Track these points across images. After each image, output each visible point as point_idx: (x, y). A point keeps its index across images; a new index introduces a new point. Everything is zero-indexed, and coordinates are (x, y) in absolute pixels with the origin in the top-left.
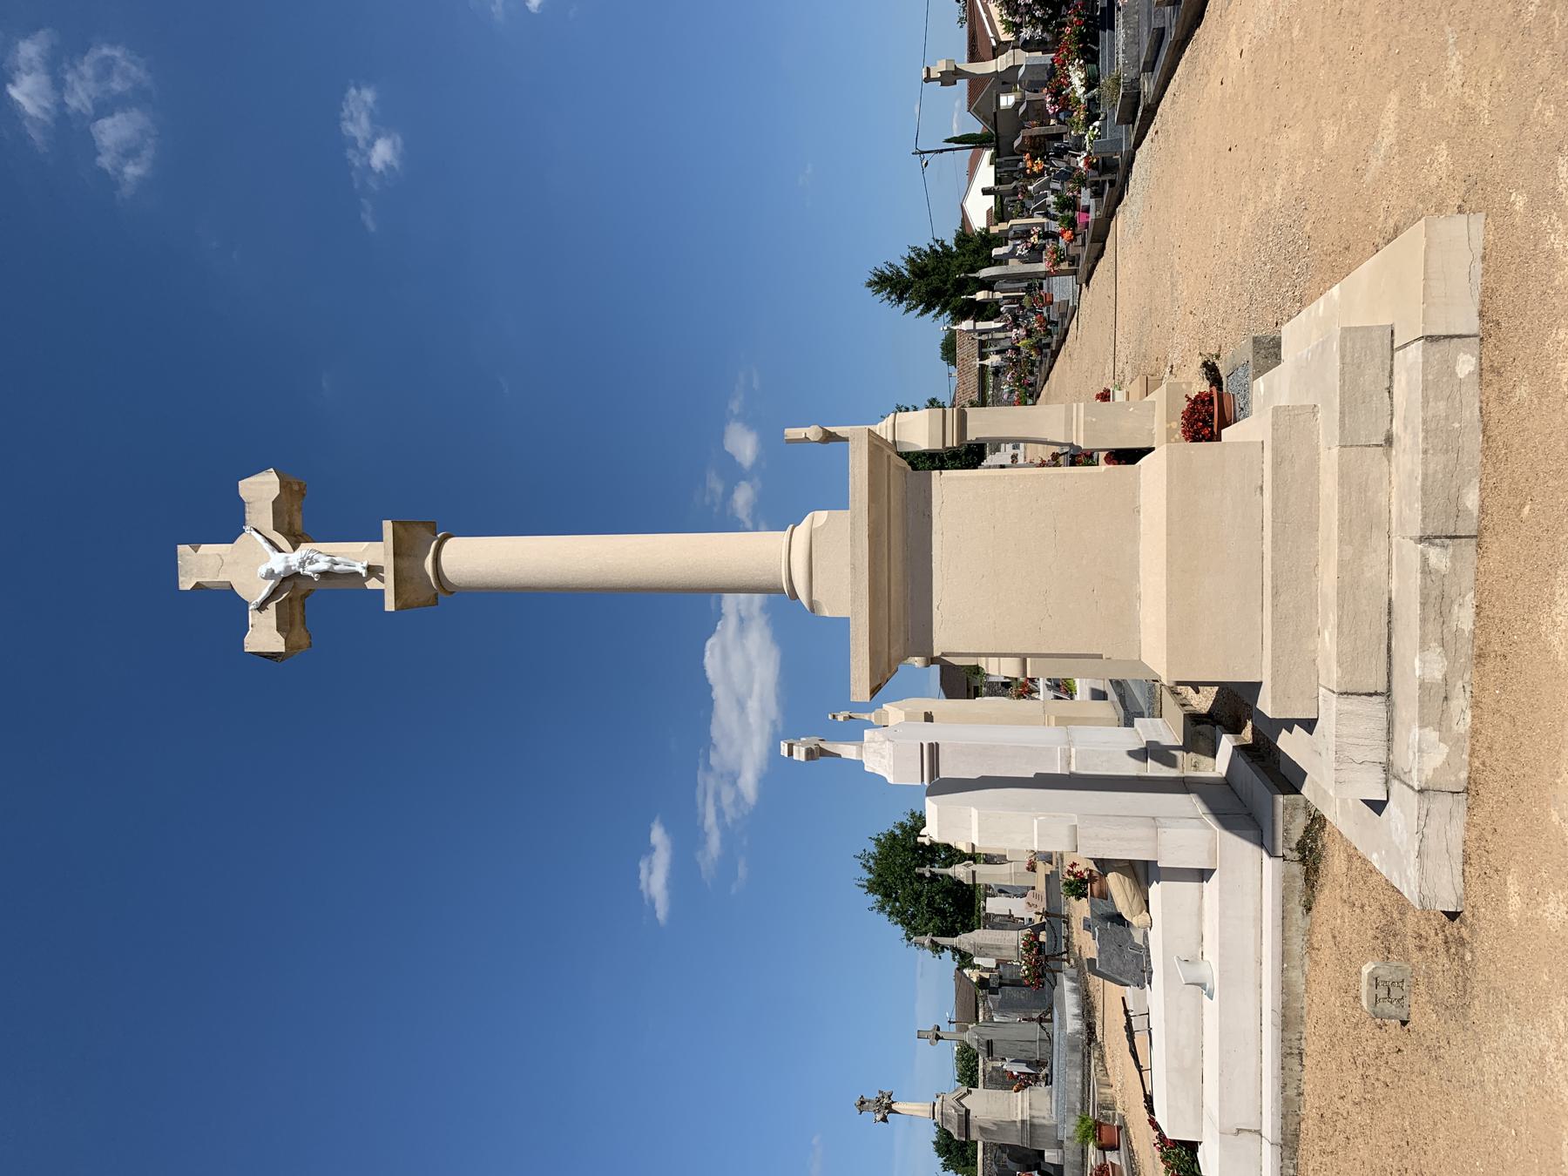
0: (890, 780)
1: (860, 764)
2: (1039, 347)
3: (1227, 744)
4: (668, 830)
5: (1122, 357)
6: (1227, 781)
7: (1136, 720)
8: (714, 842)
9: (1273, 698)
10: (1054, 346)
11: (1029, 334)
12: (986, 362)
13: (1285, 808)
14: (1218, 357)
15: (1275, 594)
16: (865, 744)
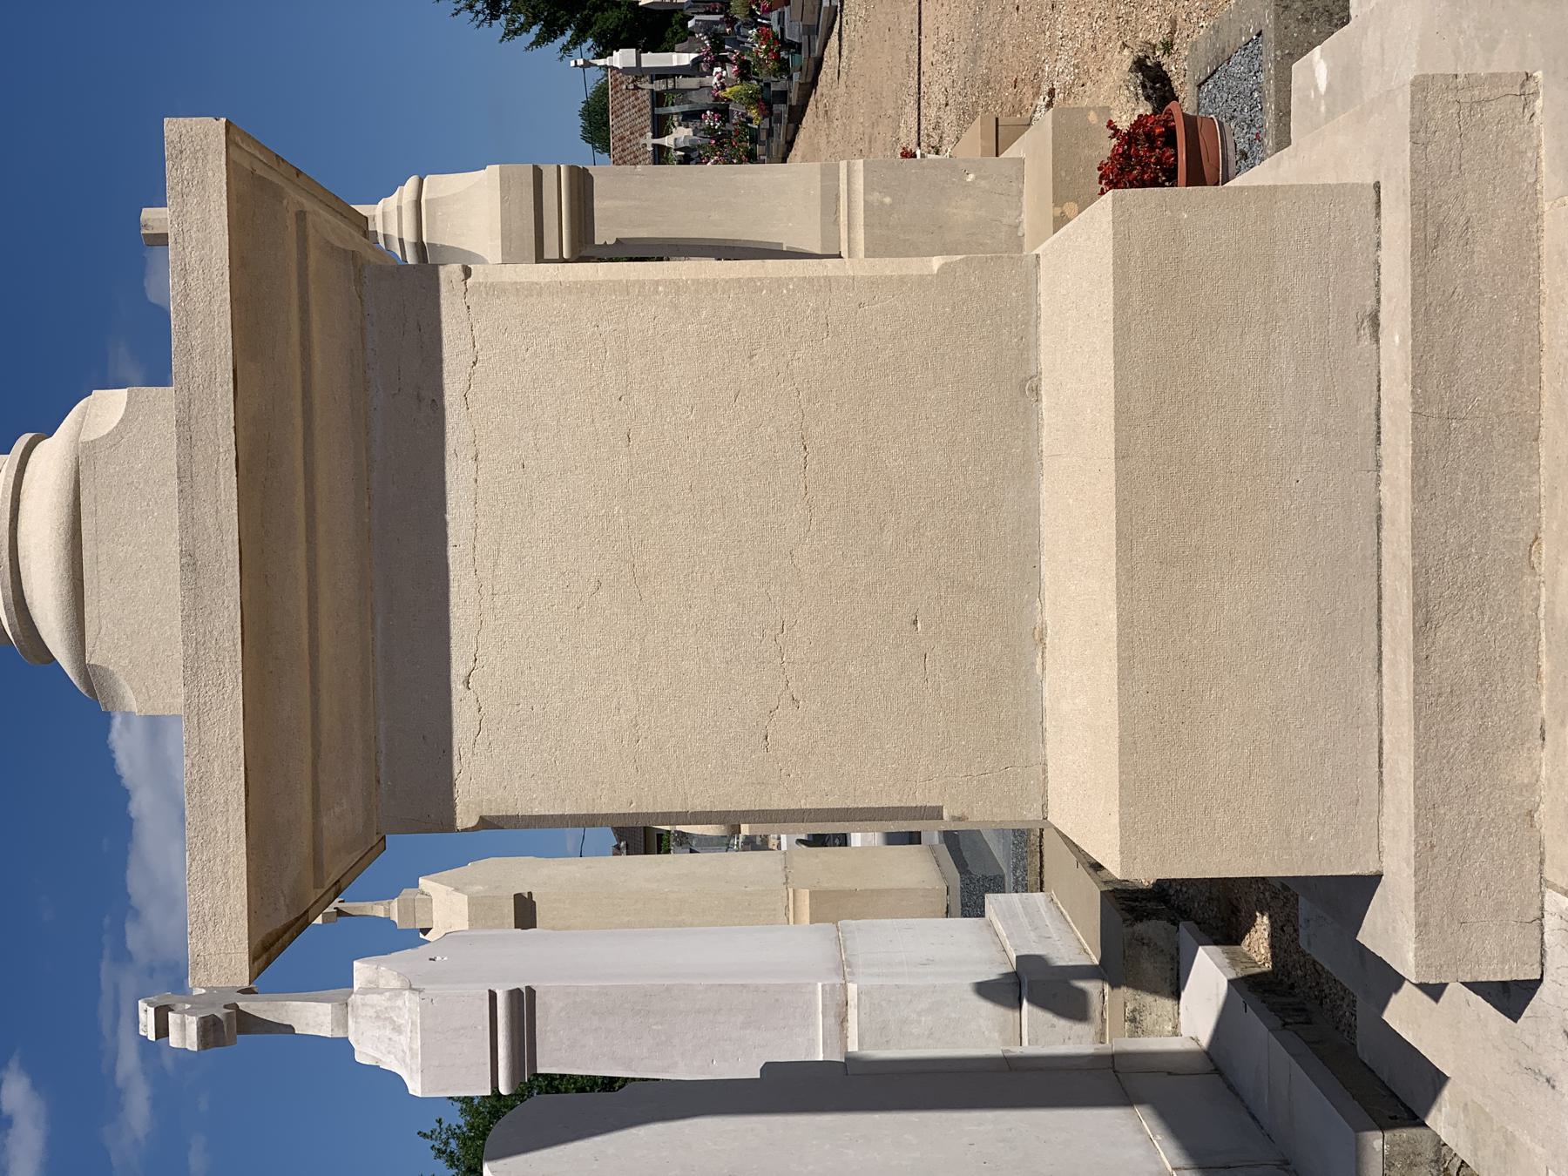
0: (415, 1088)
1: (342, 1047)
2: (766, 101)
3: (1209, 976)
4: (37, 1084)
5: (935, 93)
6: (1215, 1061)
7: (990, 898)
8: (138, 1107)
9: (1422, 926)
10: (794, 98)
11: (745, 72)
12: (667, 141)
13: (1388, 1164)
14: (1168, 47)
15: (1424, 625)
16: (355, 999)
